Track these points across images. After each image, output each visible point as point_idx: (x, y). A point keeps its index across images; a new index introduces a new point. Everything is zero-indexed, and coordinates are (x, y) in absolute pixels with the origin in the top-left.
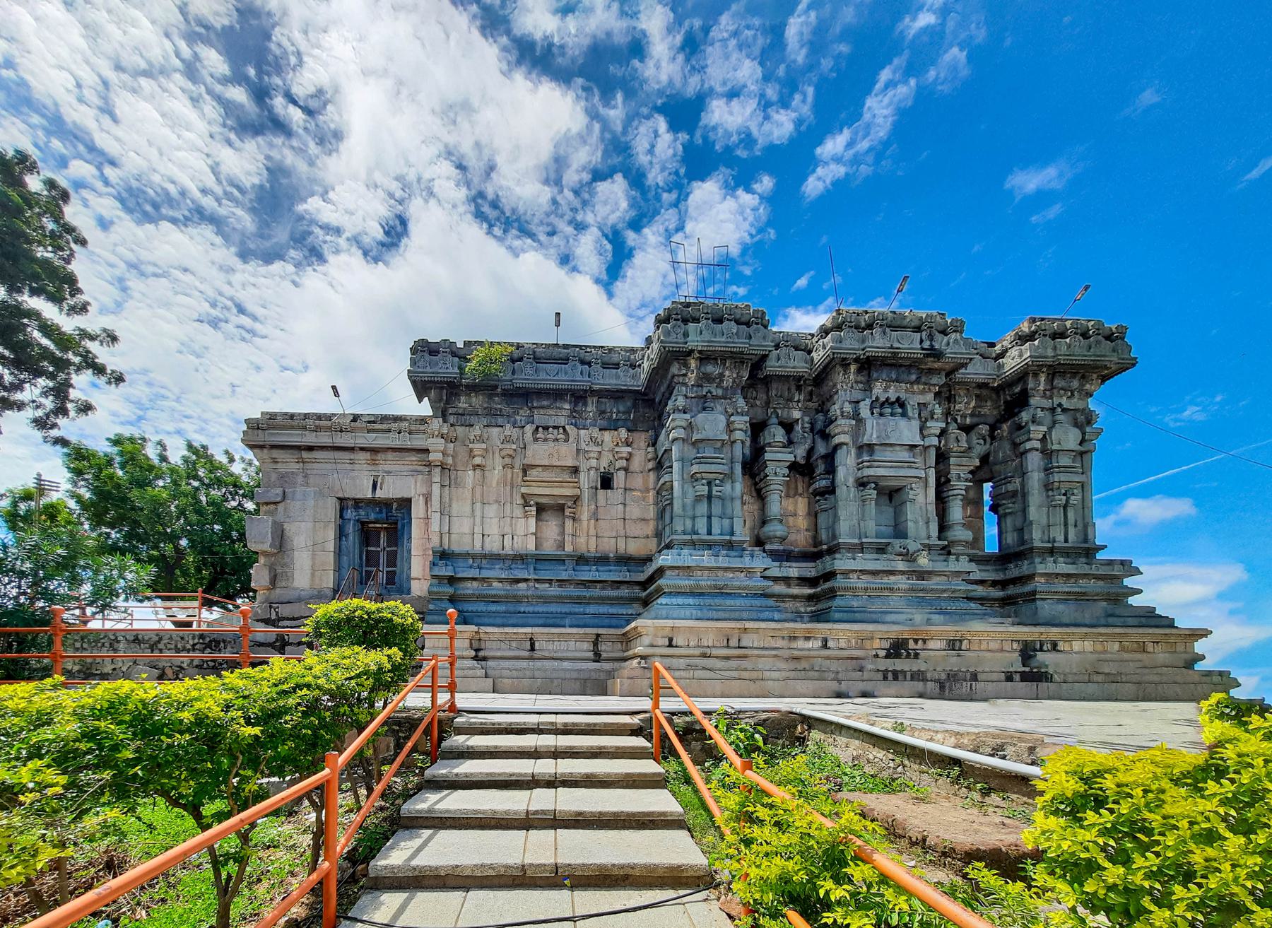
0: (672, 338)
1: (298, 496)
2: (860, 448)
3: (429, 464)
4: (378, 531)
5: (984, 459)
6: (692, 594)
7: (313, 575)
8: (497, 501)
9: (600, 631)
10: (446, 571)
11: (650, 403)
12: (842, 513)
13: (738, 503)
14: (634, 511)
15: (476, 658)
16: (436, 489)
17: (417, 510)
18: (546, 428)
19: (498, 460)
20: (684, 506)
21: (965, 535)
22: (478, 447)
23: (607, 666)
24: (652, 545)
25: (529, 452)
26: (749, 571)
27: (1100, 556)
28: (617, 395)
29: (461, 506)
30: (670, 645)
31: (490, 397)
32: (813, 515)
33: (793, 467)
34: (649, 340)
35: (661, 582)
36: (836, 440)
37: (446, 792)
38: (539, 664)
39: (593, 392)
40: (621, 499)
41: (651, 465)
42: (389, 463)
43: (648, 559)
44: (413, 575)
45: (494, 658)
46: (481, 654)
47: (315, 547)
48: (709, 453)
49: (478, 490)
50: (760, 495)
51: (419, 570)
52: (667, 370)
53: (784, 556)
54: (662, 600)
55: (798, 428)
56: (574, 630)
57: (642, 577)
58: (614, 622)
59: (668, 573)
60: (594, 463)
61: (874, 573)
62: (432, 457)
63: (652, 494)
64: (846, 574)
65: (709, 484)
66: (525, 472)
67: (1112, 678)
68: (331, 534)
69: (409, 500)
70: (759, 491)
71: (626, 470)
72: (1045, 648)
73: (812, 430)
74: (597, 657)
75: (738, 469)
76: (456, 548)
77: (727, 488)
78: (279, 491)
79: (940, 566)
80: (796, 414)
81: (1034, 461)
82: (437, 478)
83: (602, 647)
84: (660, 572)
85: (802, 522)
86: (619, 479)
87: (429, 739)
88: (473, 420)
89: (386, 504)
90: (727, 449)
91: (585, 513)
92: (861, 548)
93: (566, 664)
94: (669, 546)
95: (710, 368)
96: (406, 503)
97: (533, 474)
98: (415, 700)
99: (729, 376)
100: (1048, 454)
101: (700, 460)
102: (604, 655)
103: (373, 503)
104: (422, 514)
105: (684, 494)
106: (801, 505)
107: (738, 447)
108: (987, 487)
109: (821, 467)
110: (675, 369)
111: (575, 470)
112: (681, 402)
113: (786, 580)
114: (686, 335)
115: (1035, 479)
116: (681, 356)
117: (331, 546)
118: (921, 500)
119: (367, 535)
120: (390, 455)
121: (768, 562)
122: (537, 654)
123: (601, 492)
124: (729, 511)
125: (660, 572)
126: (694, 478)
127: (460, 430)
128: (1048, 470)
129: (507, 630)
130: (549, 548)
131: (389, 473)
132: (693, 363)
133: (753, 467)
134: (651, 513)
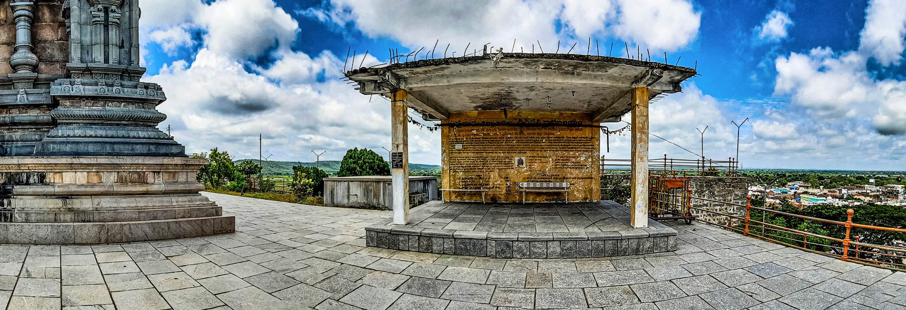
27: (145, 79)
65: (106, 10)
67: (82, 216)
72: (31, 181)
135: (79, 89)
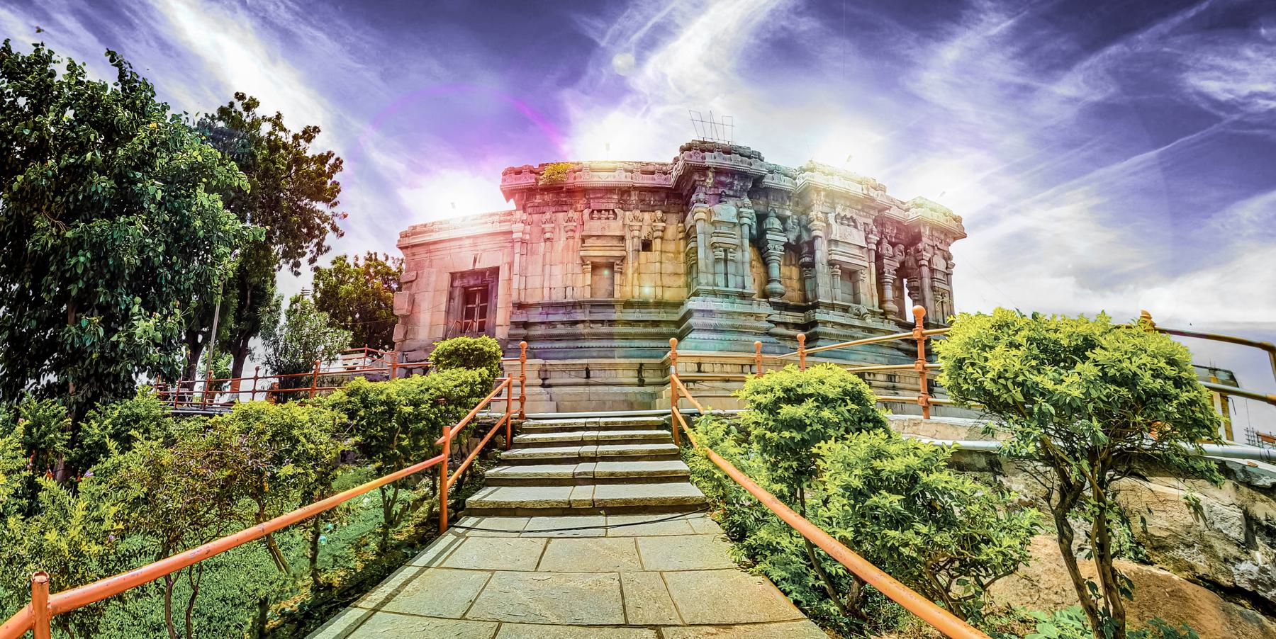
0: (694, 158)
2: (830, 241)
3: (513, 241)
4: (475, 293)
5: (902, 264)
6: (715, 331)
8: (562, 263)
9: (643, 361)
10: (521, 317)
11: (680, 196)
12: (820, 281)
13: (747, 266)
14: (668, 267)
15: (543, 386)
16: (517, 257)
17: (503, 275)
18: (599, 211)
19: (563, 235)
20: (706, 265)
21: (894, 308)
22: (548, 226)
23: (649, 389)
24: (684, 292)
25: (586, 227)
26: (757, 317)
28: (654, 190)
29: (535, 269)
30: (699, 371)
31: (558, 194)
32: (802, 280)
33: (787, 246)
34: (676, 160)
35: (691, 321)
36: (814, 233)
37: (490, 489)
38: (593, 389)
39: (635, 188)
40: (658, 258)
41: (681, 235)
43: (681, 304)
44: (498, 322)
45: (557, 385)
46: (547, 382)
47: (435, 307)
48: (724, 229)
49: (548, 255)
50: (765, 263)
51: (502, 316)
52: (691, 177)
53: (784, 307)
54: (692, 335)
55: (790, 221)
56: (622, 361)
57: (676, 318)
58: (654, 353)
59: (695, 314)
60: (636, 233)
61: (842, 325)
62: (514, 236)
63: (682, 256)
64: (825, 323)
65: (725, 251)
66: (583, 242)
68: (444, 299)
69: (498, 268)
70: (764, 259)
71: (662, 238)
73: (799, 224)
74: (642, 383)
75: (747, 242)
76: (531, 301)
77: (738, 255)
78: (414, 273)
79: (880, 326)
80: (788, 213)
81: (925, 271)
82: (517, 249)
83: (645, 374)
84: (689, 314)
85: (795, 284)
86: (657, 244)
87: (499, 440)
88: (546, 209)
89: (482, 273)
90: (737, 228)
91: (630, 269)
92: (832, 307)
93: (615, 389)
94: (696, 294)
95: (723, 178)
96: (495, 271)
97: (589, 242)
98: (497, 413)
99: (738, 184)
100: (932, 271)
101: (718, 234)
102: (647, 380)
103: (474, 273)
104: (506, 276)
105: (706, 258)
106: (794, 272)
107: (746, 229)
108: (905, 281)
109: (806, 250)
110: (696, 177)
111: (622, 238)
112: (702, 196)
113: (786, 325)
114: (704, 158)
115: (927, 281)
116: (703, 170)
117: (443, 307)
118: (867, 282)
119: (468, 296)
121: (769, 310)
122: (591, 381)
123: (643, 254)
124: (740, 272)
125: (689, 314)
126: (714, 246)
127: (535, 217)
128: (932, 278)
129: (568, 362)
130: (601, 297)
132: (710, 175)
133: (759, 242)
134: (682, 269)
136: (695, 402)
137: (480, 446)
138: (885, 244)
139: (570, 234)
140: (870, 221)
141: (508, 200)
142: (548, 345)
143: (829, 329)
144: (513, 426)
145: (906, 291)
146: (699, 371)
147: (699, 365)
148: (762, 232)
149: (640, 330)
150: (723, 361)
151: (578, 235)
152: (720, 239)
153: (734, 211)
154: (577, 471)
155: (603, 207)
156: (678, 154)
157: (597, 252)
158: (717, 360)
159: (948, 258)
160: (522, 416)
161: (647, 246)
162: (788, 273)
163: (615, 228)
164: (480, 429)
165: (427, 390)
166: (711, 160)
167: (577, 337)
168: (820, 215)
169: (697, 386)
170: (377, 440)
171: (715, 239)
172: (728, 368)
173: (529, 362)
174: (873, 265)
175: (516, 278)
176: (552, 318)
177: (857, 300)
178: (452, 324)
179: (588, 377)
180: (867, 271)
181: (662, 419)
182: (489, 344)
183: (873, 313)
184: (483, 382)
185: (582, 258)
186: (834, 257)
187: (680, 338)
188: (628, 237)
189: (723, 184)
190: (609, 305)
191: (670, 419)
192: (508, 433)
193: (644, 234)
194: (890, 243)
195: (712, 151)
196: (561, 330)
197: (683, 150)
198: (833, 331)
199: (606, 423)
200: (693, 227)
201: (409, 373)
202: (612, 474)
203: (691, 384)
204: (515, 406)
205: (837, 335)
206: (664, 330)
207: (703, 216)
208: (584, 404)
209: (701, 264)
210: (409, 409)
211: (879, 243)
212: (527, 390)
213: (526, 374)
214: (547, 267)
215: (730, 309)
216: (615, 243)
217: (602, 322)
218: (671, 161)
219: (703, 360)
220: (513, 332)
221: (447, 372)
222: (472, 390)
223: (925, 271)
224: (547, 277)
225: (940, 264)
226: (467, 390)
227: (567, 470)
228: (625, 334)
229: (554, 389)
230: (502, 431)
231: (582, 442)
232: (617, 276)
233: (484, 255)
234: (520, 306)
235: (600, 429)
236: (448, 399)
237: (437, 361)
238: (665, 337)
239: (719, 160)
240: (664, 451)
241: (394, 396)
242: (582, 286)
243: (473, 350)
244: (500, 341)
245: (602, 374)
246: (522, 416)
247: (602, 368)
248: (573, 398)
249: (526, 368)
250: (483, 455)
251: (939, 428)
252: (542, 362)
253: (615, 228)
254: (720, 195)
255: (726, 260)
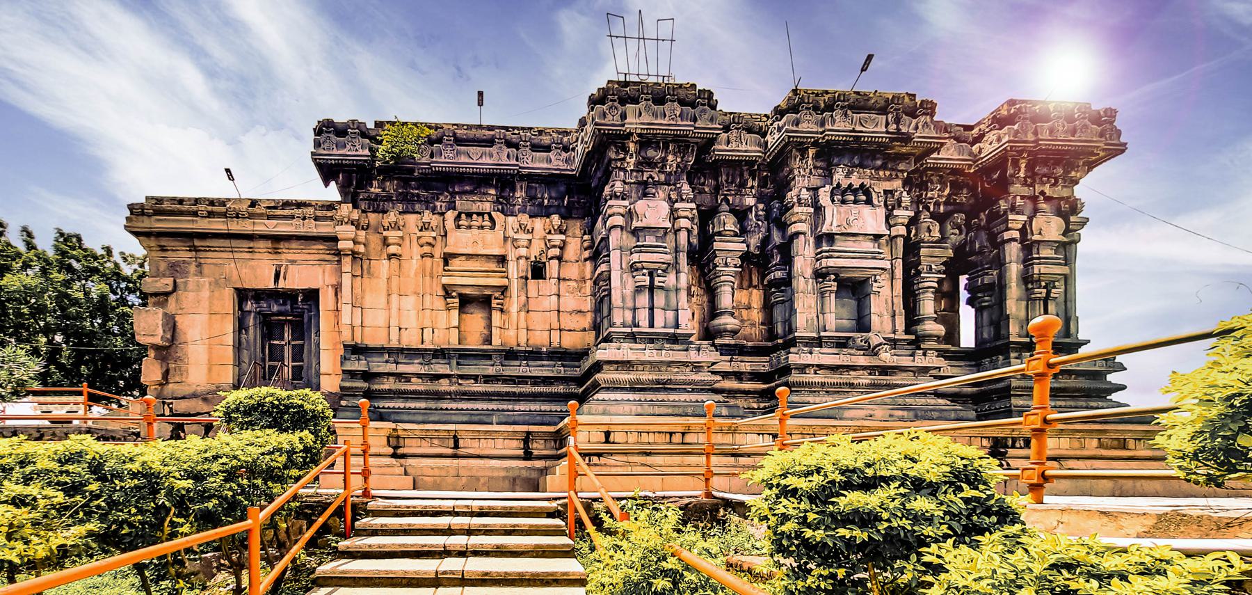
1: (191, 286)
2: (819, 239)
3: (338, 253)
5: (958, 249)
7: (210, 370)
10: (359, 365)
12: (799, 305)
13: (683, 295)
14: (569, 302)
15: (394, 456)
17: (326, 301)
18: (469, 215)
19: (417, 251)
22: (392, 235)
23: (539, 464)
25: (451, 238)
26: (697, 367)
30: (607, 441)
32: (768, 307)
34: (583, 122)
36: (793, 229)
38: (463, 462)
39: (522, 177)
40: (555, 290)
41: (587, 254)
42: (290, 253)
46: (400, 451)
47: (213, 340)
49: (395, 280)
50: (711, 293)
51: (329, 364)
54: (600, 396)
55: (752, 216)
57: (577, 372)
60: (523, 251)
62: (341, 245)
63: (589, 283)
64: (803, 369)
65: (651, 274)
68: (229, 327)
70: (708, 283)
71: (560, 259)
73: (767, 218)
74: (528, 456)
75: (683, 259)
76: (371, 343)
77: (670, 279)
78: (170, 281)
79: (906, 362)
80: (750, 201)
81: (1013, 251)
84: (598, 367)
85: (757, 315)
86: (553, 268)
88: (389, 205)
89: (289, 296)
91: (513, 304)
92: (819, 342)
94: (608, 340)
96: (312, 296)
97: (455, 264)
100: (1029, 247)
101: (640, 249)
102: (536, 453)
104: (331, 306)
106: (756, 297)
107: (683, 236)
111: (502, 260)
113: (739, 376)
114: (623, 116)
115: (1014, 270)
116: (617, 139)
117: (229, 339)
120: (294, 245)
121: (715, 356)
123: (532, 283)
125: (598, 367)
126: (634, 268)
127: (373, 218)
131: (293, 262)
133: (701, 257)
134: (588, 304)
135: (626, 351)
136: (596, 482)
137: (308, 535)
138: (925, 218)
139: (427, 249)
140: (897, 184)
141: (326, 185)
142: (400, 404)
143: (810, 377)
144: (354, 506)
145: (964, 295)
146: (607, 441)
147: (607, 434)
148: (706, 239)
149: (527, 388)
150: (641, 428)
151: (438, 252)
152: (644, 257)
153: (665, 207)
154: (442, 569)
155: (474, 208)
156: (584, 111)
157: (468, 278)
158: (633, 428)
159: (1069, 210)
160: (366, 493)
161: (538, 271)
162: (745, 301)
163: (490, 242)
164: (308, 511)
165: (216, 458)
166: (636, 120)
167: (439, 396)
168: (805, 194)
169: (603, 460)
170: (131, 525)
171: (635, 257)
172: (645, 437)
173: (373, 424)
174: (899, 264)
175: (346, 310)
176: (402, 369)
177: (862, 325)
178: (248, 368)
179: (456, 446)
180: (887, 276)
181: (554, 504)
182: (314, 400)
183: (894, 343)
184: (307, 450)
185: (444, 287)
186: (825, 262)
187: (582, 399)
188: (511, 257)
189: (650, 163)
190: (486, 356)
191: (565, 506)
192: (350, 515)
193: (535, 252)
194: (934, 216)
195: (635, 101)
196: (416, 385)
197: (594, 101)
198: (818, 379)
199: (481, 508)
200: (605, 240)
201: (177, 432)
202: (486, 574)
203: (595, 459)
204: (356, 482)
205: (823, 385)
206: (560, 389)
207: (619, 220)
208: (450, 480)
209: (616, 298)
210: (188, 484)
211: (913, 222)
212: (372, 461)
213: (371, 441)
214: (394, 298)
215: (657, 358)
216: (493, 266)
217: (475, 378)
218: (575, 125)
219: (613, 428)
220: (347, 384)
221: (248, 435)
222: (289, 459)
223: (1013, 251)
224: (394, 311)
225: (1049, 227)
226: (283, 459)
227: (427, 566)
228: (508, 394)
229: (410, 461)
230: (339, 512)
231: (449, 532)
232: (496, 315)
233: (293, 269)
234: (356, 350)
235: (472, 514)
236: (252, 470)
237: (229, 419)
238: (564, 398)
239: (646, 118)
240: (554, 546)
241: (157, 466)
242: (445, 327)
243: (287, 407)
244: (328, 396)
245: (475, 443)
246: (366, 493)
247: (477, 436)
248: (437, 472)
249: (370, 432)
250: (312, 544)
251: (1065, 518)
252: (393, 425)
253: (490, 242)
254: (644, 184)
255: (651, 288)
